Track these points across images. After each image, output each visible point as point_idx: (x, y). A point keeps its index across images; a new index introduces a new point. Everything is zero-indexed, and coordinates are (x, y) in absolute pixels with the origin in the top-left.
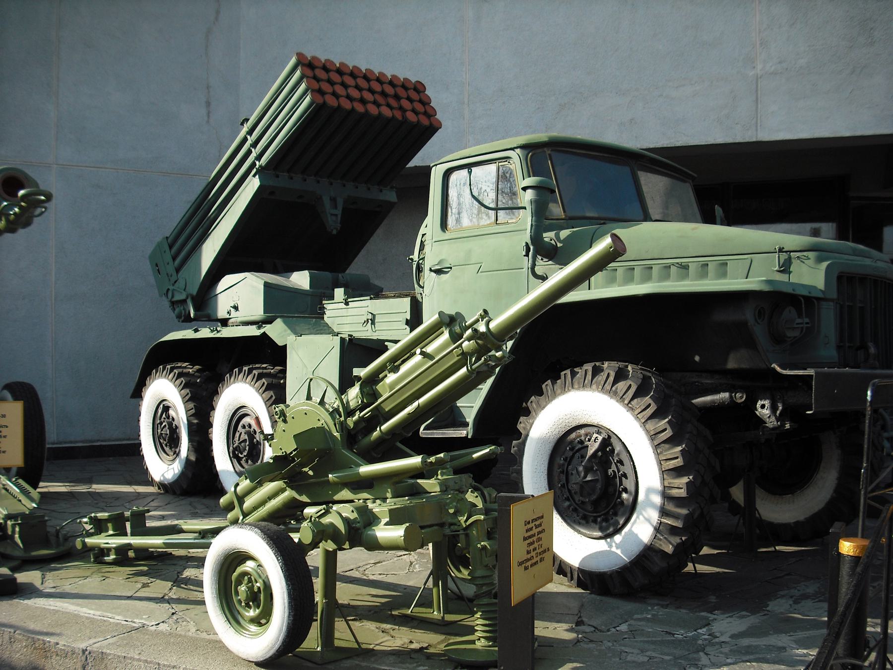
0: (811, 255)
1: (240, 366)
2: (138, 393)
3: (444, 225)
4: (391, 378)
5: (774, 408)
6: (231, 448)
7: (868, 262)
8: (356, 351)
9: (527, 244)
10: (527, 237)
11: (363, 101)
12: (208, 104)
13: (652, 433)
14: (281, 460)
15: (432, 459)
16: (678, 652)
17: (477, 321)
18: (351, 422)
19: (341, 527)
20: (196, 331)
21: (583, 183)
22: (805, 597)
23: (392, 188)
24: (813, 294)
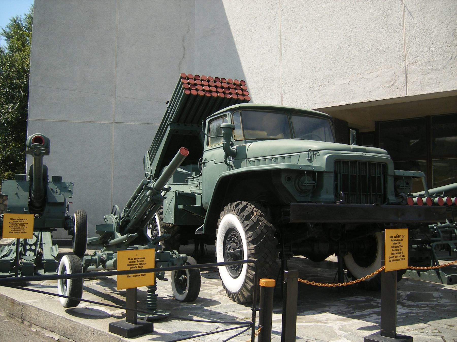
7: (356, 153)
24: (323, 170)
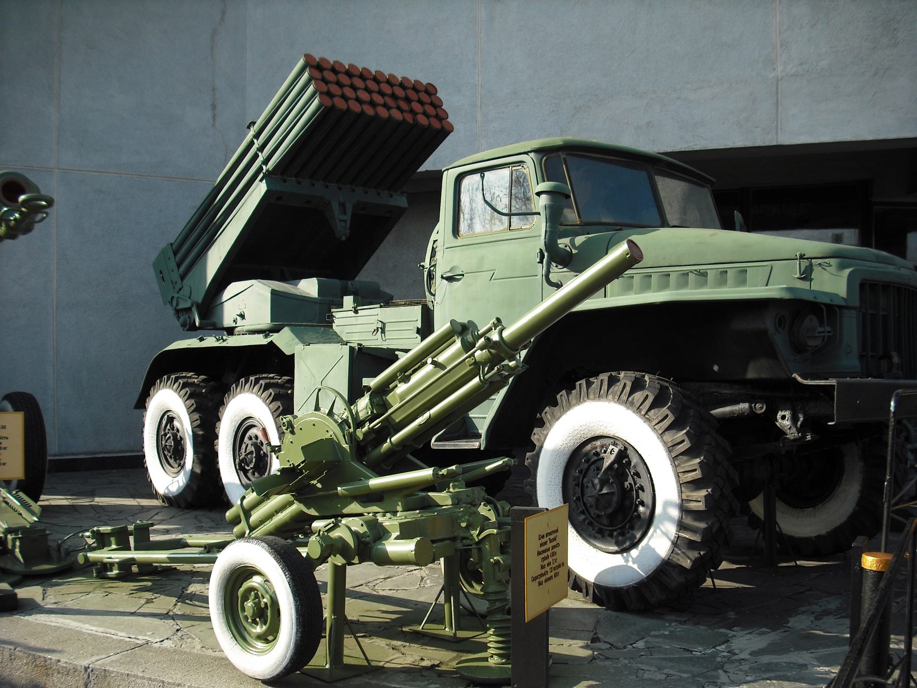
0: (833, 261)
1: (246, 375)
2: (141, 404)
3: (456, 231)
4: (402, 388)
5: (794, 419)
6: (237, 460)
7: (891, 269)
8: (366, 361)
9: (541, 250)
10: (541, 243)
11: (372, 104)
12: (214, 107)
13: (670, 444)
14: (288, 473)
15: (444, 471)
16: (696, 670)
17: (490, 330)
18: (360, 433)
19: (350, 541)
20: (201, 340)
21: (598, 188)
22: (827, 613)
23: (402, 193)
24: (835, 302)
